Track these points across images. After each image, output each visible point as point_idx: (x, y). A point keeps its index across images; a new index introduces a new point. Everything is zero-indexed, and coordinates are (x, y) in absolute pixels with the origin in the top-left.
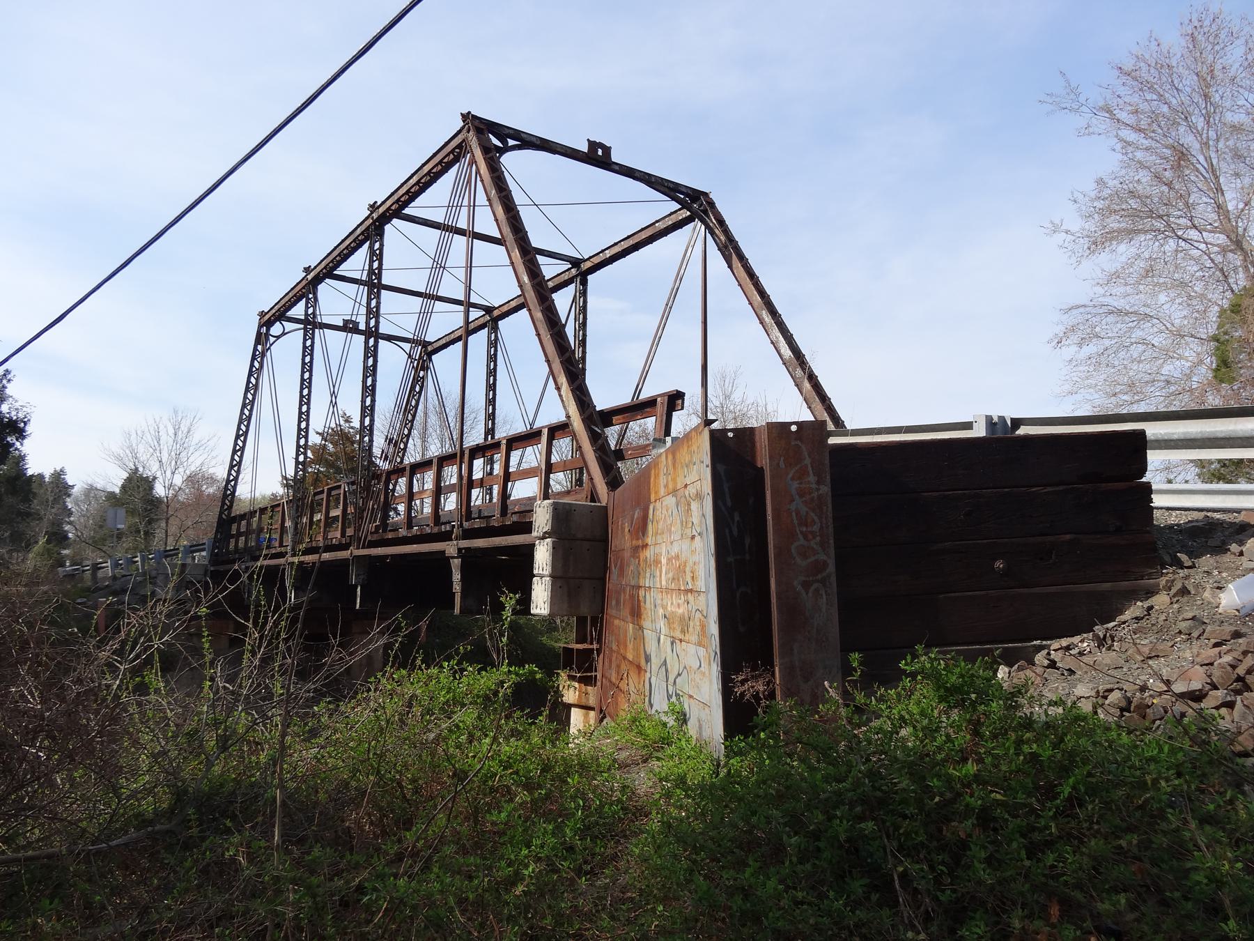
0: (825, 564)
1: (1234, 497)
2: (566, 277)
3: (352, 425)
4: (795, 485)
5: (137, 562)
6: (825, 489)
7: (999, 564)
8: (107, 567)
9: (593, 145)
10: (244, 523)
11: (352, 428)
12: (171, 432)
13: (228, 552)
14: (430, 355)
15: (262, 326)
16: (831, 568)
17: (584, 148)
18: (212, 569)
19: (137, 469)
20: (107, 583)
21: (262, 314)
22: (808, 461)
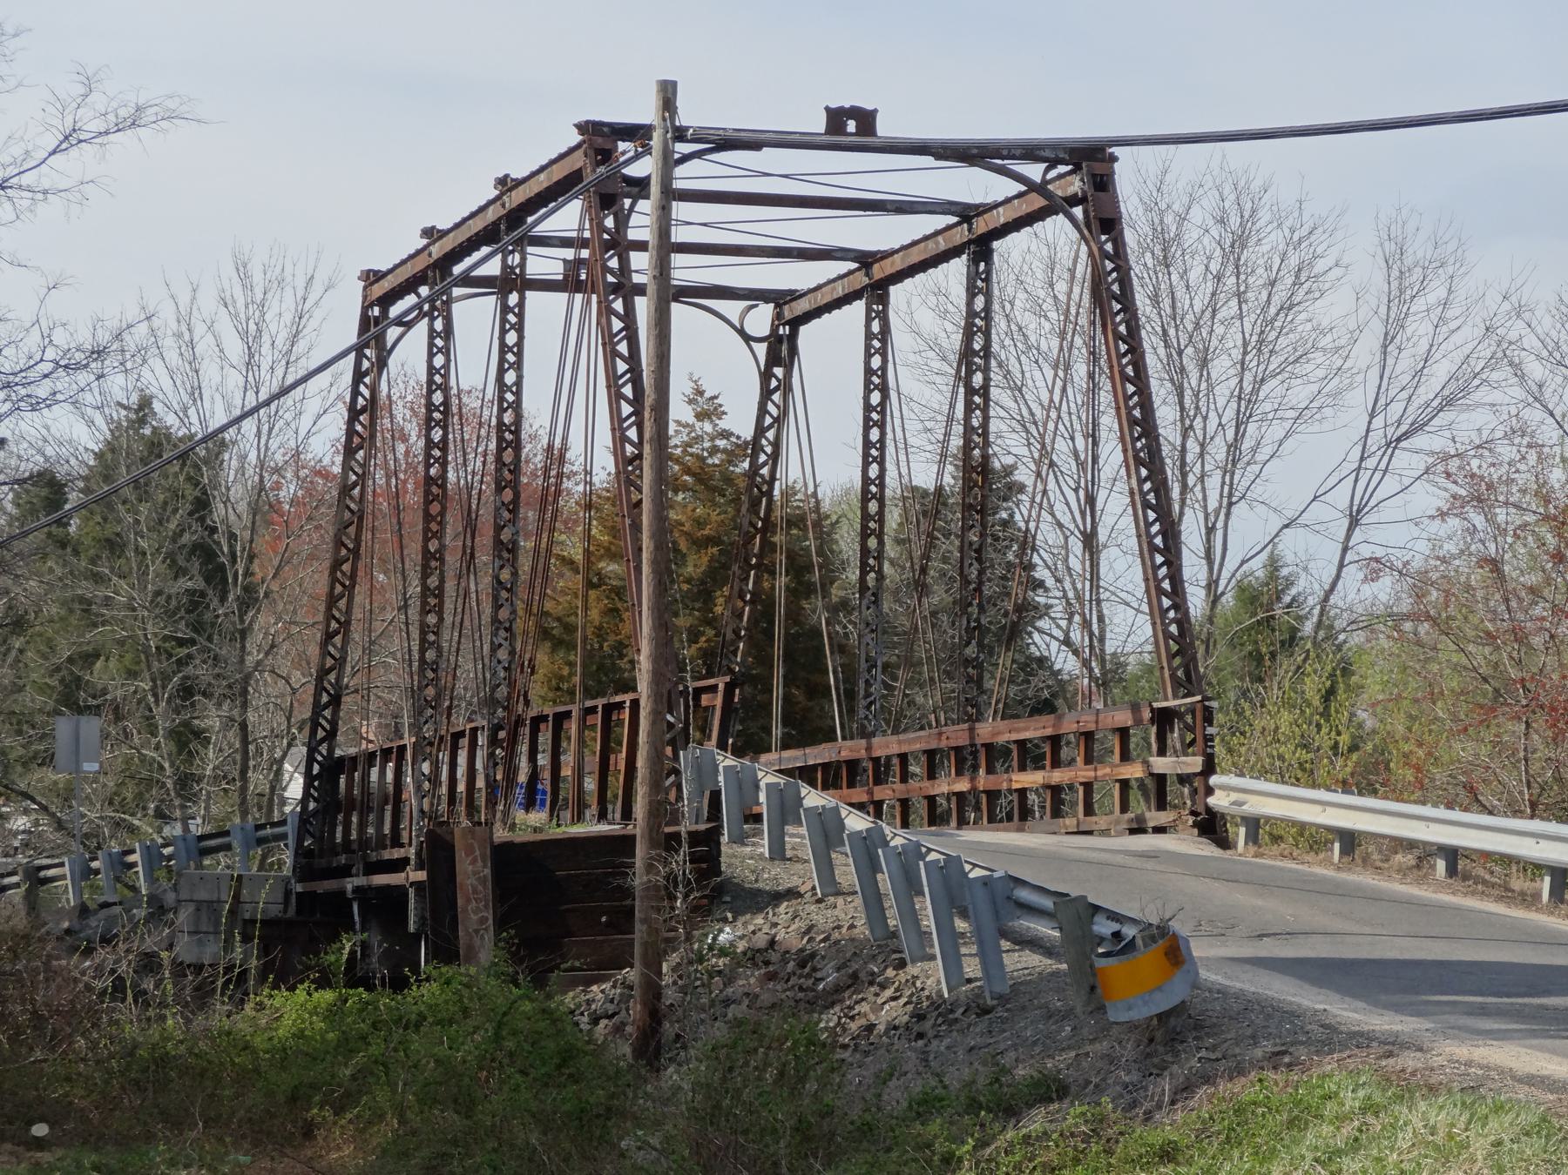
0: (487, 919)
1: (1421, 825)
2: (942, 244)
3: (723, 424)
4: (470, 868)
5: (134, 865)
6: (487, 871)
7: (604, 919)
8: (63, 877)
9: (836, 118)
10: (312, 791)
11: (726, 434)
12: (235, 349)
13: (334, 851)
14: (797, 322)
15: (371, 305)
16: (491, 921)
17: (818, 124)
18: (299, 888)
19: (145, 403)
20: (66, 925)
21: (371, 277)
22: (478, 853)
